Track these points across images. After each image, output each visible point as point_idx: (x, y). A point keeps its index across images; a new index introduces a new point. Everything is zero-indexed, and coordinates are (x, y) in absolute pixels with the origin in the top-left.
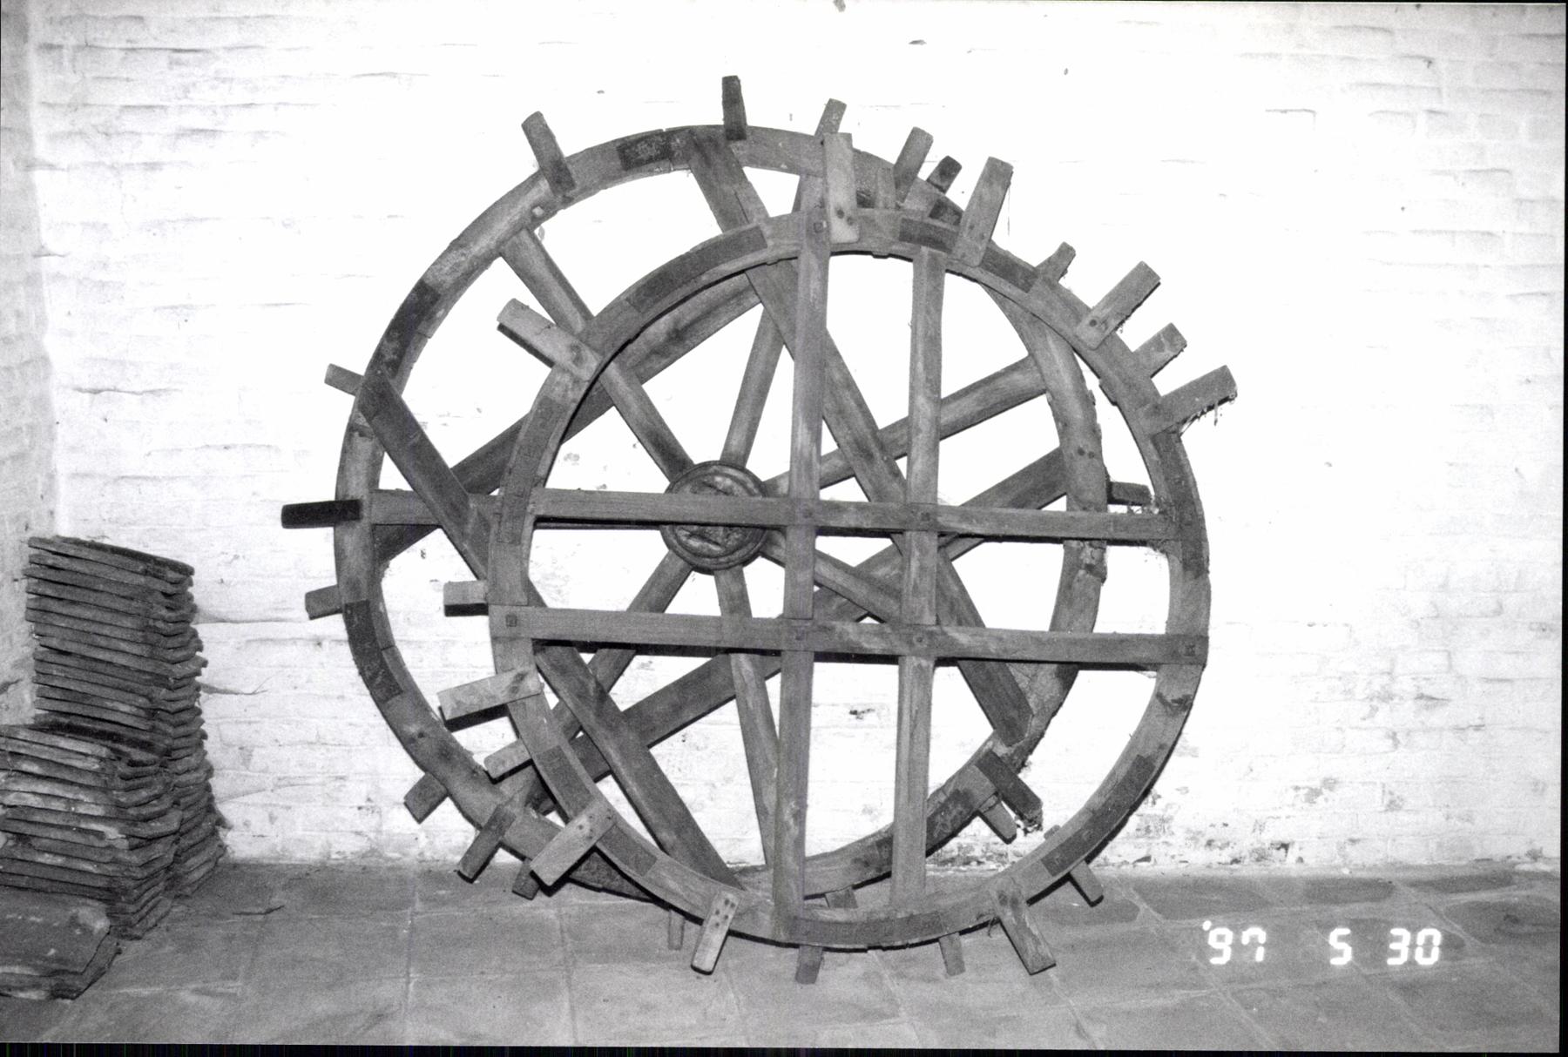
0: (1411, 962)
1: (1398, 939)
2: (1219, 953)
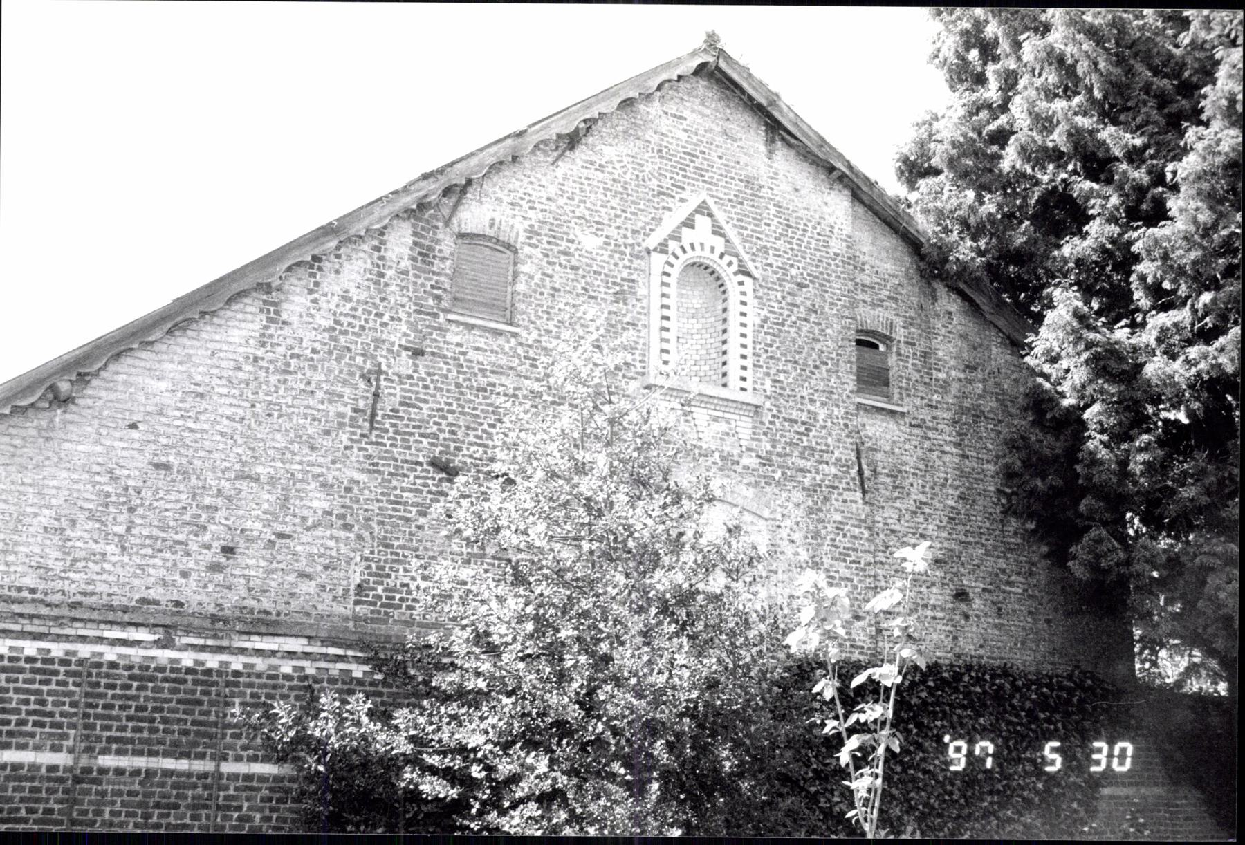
1: (1099, 750)
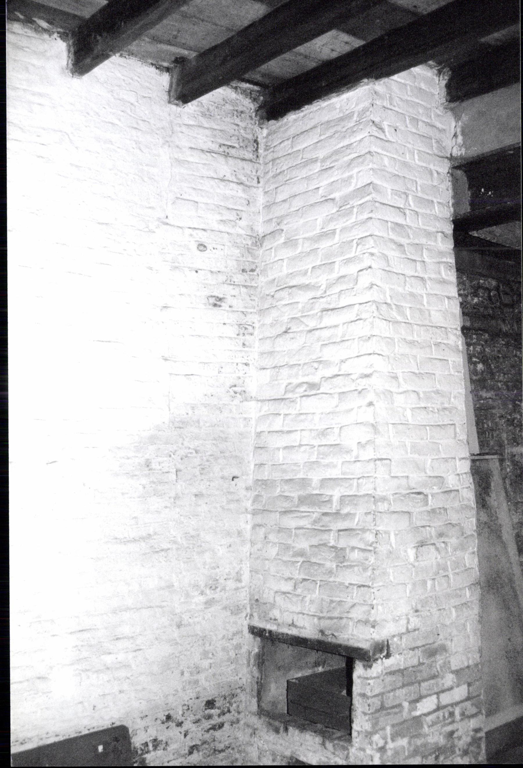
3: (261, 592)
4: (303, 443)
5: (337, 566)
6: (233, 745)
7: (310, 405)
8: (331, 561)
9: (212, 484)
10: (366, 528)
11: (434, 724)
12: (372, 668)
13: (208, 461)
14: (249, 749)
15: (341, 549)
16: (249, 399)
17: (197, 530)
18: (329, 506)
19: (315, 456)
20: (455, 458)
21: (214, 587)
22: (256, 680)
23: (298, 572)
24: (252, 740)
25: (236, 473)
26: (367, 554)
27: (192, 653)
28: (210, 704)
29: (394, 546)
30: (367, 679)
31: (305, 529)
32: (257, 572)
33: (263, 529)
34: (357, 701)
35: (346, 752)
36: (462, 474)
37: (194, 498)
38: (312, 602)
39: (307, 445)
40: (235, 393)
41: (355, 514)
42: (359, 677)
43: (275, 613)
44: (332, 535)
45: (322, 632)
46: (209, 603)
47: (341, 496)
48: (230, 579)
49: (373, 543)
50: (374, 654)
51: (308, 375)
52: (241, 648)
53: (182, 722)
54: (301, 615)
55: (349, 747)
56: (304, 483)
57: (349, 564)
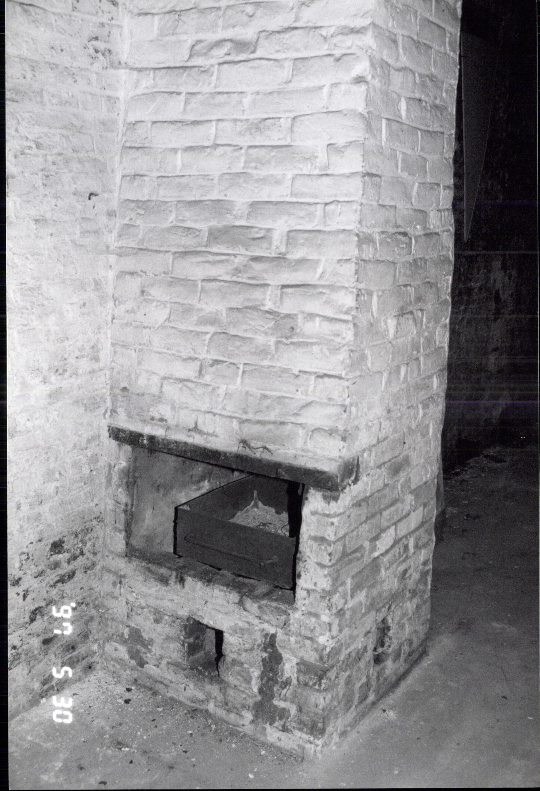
0: (54, 709)
1: (67, 701)
2: (58, 611)
3: (133, 376)
4: (218, 142)
5: (278, 343)
6: (88, 600)
7: (235, 78)
8: (266, 333)
9: (60, 203)
10: (338, 284)
11: (391, 563)
12: (339, 501)
13: (54, 163)
14: (110, 603)
15: (288, 316)
16: (116, 64)
17: (38, 279)
18: (265, 245)
19: (242, 164)
20: (438, 185)
21: (61, 371)
22: (123, 507)
23: (206, 348)
24: (117, 591)
25: (94, 189)
26: (338, 326)
27: (31, 474)
28: (57, 546)
29: (375, 315)
30: (328, 516)
31: (220, 281)
32: (125, 346)
33: (139, 279)
34: (307, 545)
35: (283, 618)
36: (444, 210)
37: (33, 226)
38: (228, 395)
39: (229, 145)
40: (97, 51)
41: (318, 262)
42: (314, 513)
43: (165, 411)
44: (269, 292)
45: (244, 442)
46: (55, 395)
47: (290, 231)
48: (82, 357)
49: (351, 309)
50: (342, 481)
51: (234, 27)
52: (97, 461)
53: (20, 579)
54: (209, 416)
55: (290, 611)
56: (220, 207)
57: (301, 340)
